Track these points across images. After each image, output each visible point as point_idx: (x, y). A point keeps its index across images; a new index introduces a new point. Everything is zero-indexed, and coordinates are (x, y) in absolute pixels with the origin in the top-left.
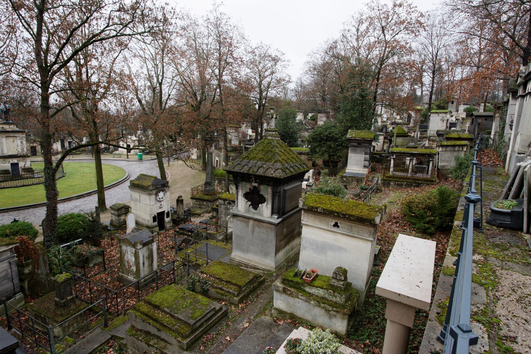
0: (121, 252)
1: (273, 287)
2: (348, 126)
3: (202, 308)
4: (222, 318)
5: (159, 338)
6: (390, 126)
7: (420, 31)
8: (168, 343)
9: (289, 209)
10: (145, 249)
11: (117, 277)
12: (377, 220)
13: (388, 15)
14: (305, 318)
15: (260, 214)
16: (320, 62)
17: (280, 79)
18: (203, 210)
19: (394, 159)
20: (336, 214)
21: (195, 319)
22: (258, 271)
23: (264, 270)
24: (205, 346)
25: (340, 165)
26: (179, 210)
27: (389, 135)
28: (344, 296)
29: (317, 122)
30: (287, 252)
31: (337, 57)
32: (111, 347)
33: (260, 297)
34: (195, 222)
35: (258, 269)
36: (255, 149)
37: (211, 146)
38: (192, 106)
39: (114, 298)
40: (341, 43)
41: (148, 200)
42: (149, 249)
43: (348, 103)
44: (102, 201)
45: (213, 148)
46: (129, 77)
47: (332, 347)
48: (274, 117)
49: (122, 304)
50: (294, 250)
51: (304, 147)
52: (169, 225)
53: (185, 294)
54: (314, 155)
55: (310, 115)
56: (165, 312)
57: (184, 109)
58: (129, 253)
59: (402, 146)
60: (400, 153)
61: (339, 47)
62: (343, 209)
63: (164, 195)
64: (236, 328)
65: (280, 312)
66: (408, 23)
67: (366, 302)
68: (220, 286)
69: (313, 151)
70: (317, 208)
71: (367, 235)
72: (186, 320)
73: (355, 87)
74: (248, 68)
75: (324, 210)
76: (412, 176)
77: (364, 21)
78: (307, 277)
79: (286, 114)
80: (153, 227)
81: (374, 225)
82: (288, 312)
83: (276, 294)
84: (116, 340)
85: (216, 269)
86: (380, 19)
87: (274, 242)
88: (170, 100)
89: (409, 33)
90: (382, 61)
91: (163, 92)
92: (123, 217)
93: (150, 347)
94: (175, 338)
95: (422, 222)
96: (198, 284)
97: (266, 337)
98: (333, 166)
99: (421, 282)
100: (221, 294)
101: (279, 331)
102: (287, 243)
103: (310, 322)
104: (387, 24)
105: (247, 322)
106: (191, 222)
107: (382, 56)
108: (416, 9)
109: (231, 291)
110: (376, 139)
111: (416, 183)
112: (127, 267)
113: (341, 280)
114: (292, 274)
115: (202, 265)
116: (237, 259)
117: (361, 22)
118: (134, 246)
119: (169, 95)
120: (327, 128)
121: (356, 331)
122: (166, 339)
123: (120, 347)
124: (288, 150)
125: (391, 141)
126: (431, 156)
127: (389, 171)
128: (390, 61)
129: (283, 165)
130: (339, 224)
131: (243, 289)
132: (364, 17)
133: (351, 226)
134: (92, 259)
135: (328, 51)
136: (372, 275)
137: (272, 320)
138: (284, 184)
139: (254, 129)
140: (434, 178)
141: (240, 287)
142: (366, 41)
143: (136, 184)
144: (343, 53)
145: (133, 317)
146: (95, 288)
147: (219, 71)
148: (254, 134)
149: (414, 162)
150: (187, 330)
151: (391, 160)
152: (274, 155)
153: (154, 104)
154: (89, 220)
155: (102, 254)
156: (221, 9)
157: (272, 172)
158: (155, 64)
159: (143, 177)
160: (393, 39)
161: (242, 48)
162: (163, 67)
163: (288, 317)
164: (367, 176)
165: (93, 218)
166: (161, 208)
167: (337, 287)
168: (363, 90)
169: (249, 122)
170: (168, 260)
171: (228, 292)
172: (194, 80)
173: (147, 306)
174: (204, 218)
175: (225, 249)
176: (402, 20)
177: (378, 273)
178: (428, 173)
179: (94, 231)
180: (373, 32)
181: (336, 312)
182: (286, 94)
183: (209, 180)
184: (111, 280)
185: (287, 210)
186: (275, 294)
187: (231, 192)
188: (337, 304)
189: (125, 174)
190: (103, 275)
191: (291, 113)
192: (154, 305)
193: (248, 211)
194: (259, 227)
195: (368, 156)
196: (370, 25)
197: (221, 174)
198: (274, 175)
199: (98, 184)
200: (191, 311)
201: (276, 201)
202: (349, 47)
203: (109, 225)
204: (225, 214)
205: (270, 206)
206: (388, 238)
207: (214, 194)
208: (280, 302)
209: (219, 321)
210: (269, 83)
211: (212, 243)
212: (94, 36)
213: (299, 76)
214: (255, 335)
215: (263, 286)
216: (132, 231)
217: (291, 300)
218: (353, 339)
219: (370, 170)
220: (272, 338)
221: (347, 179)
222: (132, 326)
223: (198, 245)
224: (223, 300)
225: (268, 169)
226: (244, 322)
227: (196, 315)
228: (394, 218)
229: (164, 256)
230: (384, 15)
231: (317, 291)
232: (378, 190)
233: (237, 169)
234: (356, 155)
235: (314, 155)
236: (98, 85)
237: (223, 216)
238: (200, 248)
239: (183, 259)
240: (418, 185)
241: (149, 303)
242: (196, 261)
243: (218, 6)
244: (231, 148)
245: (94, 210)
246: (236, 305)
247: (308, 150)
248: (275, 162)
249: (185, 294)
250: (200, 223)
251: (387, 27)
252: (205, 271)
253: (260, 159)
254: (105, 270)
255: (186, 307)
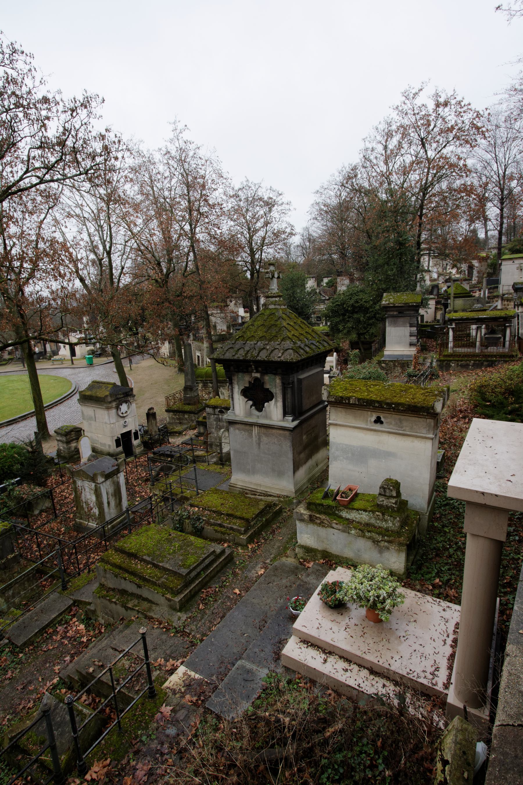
0: (76, 489)
1: (295, 516)
3: (196, 553)
6: (442, 285)
7: (479, 140)
8: (154, 603)
10: (108, 482)
11: (74, 525)
12: (438, 407)
13: (428, 121)
14: (345, 556)
15: (267, 417)
16: (334, 202)
17: (279, 231)
18: (185, 426)
19: (453, 328)
20: (377, 405)
21: (188, 568)
22: (271, 498)
23: (279, 496)
24: (206, 604)
25: (374, 346)
26: (151, 428)
27: (443, 298)
28: (398, 519)
29: (336, 288)
30: (310, 469)
31: (359, 190)
32: (74, 616)
33: (276, 533)
34: (174, 443)
35: (271, 496)
38: (157, 281)
39: (72, 554)
40: (363, 170)
41: (107, 417)
42: (114, 483)
44: (42, 425)
46: (64, 246)
47: (387, 587)
49: (84, 562)
50: (320, 467)
51: (321, 326)
52: (140, 450)
53: (170, 535)
54: (336, 335)
55: (326, 280)
56: (145, 561)
57: (146, 285)
58: (87, 490)
59: (464, 310)
60: (462, 319)
61: (359, 176)
62: (387, 396)
63: (129, 408)
64: (246, 577)
65: (308, 550)
66: (459, 129)
67: (431, 528)
68: (219, 522)
69: (334, 330)
70: (349, 398)
71: (424, 431)
72: (175, 569)
73: (388, 231)
74: (232, 220)
75: (359, 400)
76: (482, 352)
77: (394, 134)
78: (342, 497)
80: (118, 454)
81: (434, 415)
82: (320, 548)
83: (299, 525)
84: (80, 606)
85: (211, 499)
86: (416, 128)
87: (290, 456)
88: (124, 274)
89: (461, 145)
90: (424, 189)
91: (114, 265)
92: (73, 445)
94: (163, 596)
95: (503, 411)
96: (187, 521)
97: (291, 586)
98: (365, 349)
99: (514, 475)
101: (308, 575)
102: (309, 457)
104: (429, 133)
105: (261, 568)
106: (169, 443)
107: (424, 182)
108: (469, 107)
109: (235, 527)
110: (423, 304)
111: (488, 361)
112: (86, 510)
114: (320, 495)
117: (389, 135)
118: (93, 479)
119: (123, 268)
120: (351, 294)
121: (420, 568)
122: (150, 598)
123: (86, 614)
124: (299, 322)
125: (446, 306)
126: (508, 319)
127: (447, 347)
128: (437, 188)
129: (295, 343)
130: (382, 419)
131: (252, 523)
132: (394, 127)
133: (400, 420)
134: (37, 504)
135: (345, 182)
136: (436, 491)
137: (297, 562)
139: (247, 307)
140: (513, 351)
141: (247, 520)
142: (399, 162)
143: (88, 396)
144: (366, 185)
145: (102, 572)
146: (45, 542)
148: (248, 315)
149: (483, 331)
151: (448, 333)
152: (280, 330)
153: (103, 283)
154: (28, 451)
155: (50, 495)
156: (186, 136)
157: (280, 355)
158: (98, 226)
159: (95, 385)
160: (438, 156)
161: (220, 190)
162: (110, 228)
163: (319, 556)
164: (416, 357)
165: (32, 447)
166: (125, 426)
167: (387, 507)
168: (400, 235)
169: (239, 298)
171: (232, 529)
172: (155, 244)
173: (118, 555)
174: (187, 437)
175: (220, 473)
176: (450, 126)
177: (443, 487)
178: (504, 346)
179: (35, 466)
180: (410, 147)
181: (389, 542)
182: (288, 254)
183: (189, 384)
184: (65, 530)
186: (298, 524)
188: (388, 531)
189: (71, 386)
190: (54, 525)
191: (298, 279)
192: (129, 553)
193: (250, 415)
194: (267, 435)
195: (415, 328)
196: (403, 138)
198: (282, 358)
199: (35, 402)
200: (181, 558)
201: (289, 396)
202: (374, 174)
203: (55, 457)
204: (217, 427)
205: (280, 404)
206: (454, 439)
207: (199, 402)
208: (306, 536)
209: (222, 569)
210: (264, 239)
211: (201, 467)
212: (10, 188)
213: (305, 225)
215: (280, 518)
216: (89, 460)
217: (322, 532)
218: (416, 579)
219: (419, 348)
221: (387, 364)
222: (101, 584)
223: (183, 472)
224: (225, 541)
225: (272, 351)
226: (257, 568)
227: (189, 562)
228: (461, 411)
230: (422, 122)
231: (358, 516)
232: (433, 375)
233: (228, 356)
234: (398, 329)
236: (22, 258)
237: (213, 430)
239: (163, 492)
240: (491, 364)
241: (121, 551)
242: (182, 492)
243: (181, 132)
244: (217, 337)
245: (33, 437)
246: (244, 547)
247: (327, 329)
248: (282, 340)
249: (170, 535)
250: (182, 443)
251: (429, 139)
252: (196, 503)
253: (261, 338)
254: (56, 516)
255: (174, 552)
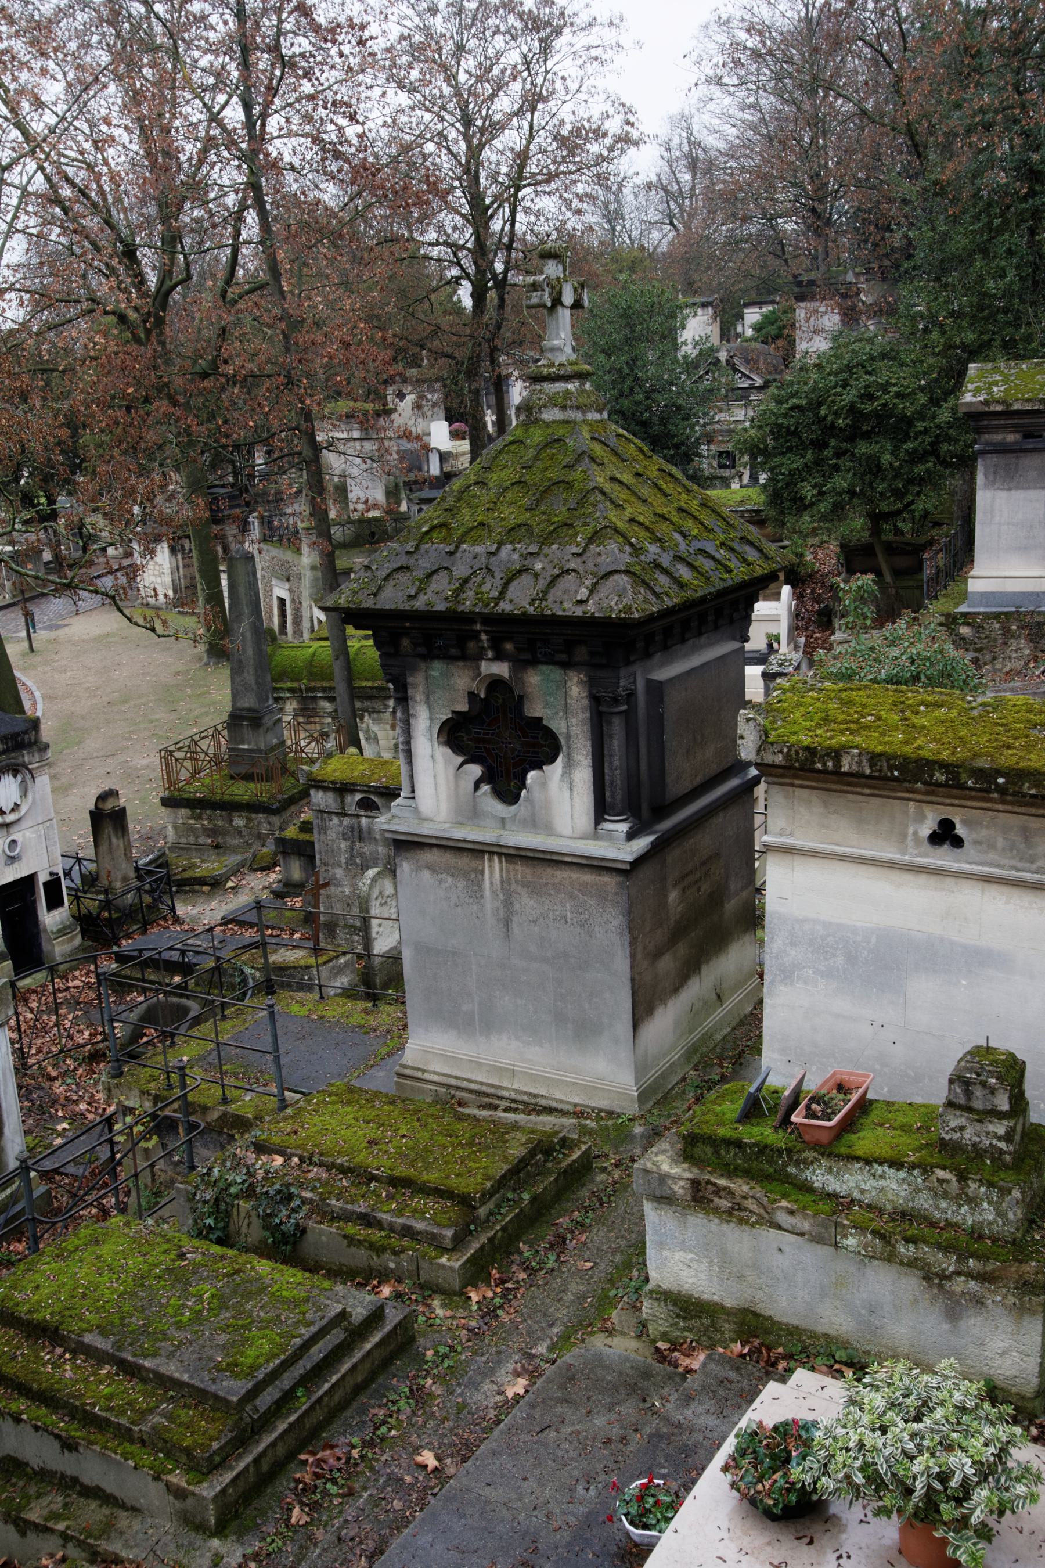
1: (638, 1183)
2: (964, 347)
3: (277, 1321)
4: (386, 1363)
5: (69, 1484)
8: (123, 1506)
9: (685, 785)
14: (822, 1327)
15: (535, 823)
17: (577, 131)
18: (235, 859)
20: (939, 777)
23: (580, 1113)
24: (315, 1506)
25: (932, 562)
28: (1016, 1194)
29: (792, 343)
30: (696, 1013)
33: (571, 1245)
34: (195, 920)
35: (550, 1110)
36: (481, 483)
37: (244, 527)
38: (122, 318)
43: (955, 220)
45: (256, 532)
47: (976, 1443)
48: (568, 298)
50: (729, 1004)
51: (735, 486)
52: (67, 948)
53: (182, 1256)
54: (790, 520)
55: (753, 316)
56: (88, 1351)
63: (24, 793)
64: (463, 1406)
68: (361, 1207)
70: (836, 754)
72: (202, 1381)
73: (988, 127)
74: (401, 86)
75: (874, 758)
78: (810, 1114)
79: (626, 315)
82: (729, 1303)
87: (622, 964)
93: (31, 1536)
94: (157, 1478)
96: (244, 1205)
98: (897, 573)
100: (372, 1246)
101: (688, 1399)
102: (691, 967)
103: (845, 1345)
105: (517, 1374)
106: (177, 920)
109: (420, 1226)
113: (995, 1114)
114: (731, 1108)
115: (259, 1118)
116: (437, 1068)
120: (849, 368)
122: (109, 1488)
124: (653, 473)
129: (637, 551)
130: (960, 830)
137: (649, 1352)
138: (648, 655)
141: (464, 1201)
147: (247, 107)
148: (465, 446)
150: (213, 1429)
152: (582, 502)
166: (12, 860)
167: (978, 1153)
169: (429, 382)
170: (74, 1118)
171: (407, 1232)
174: (243, 899)
175: (365, 1030)
181: (983, 1278)
182: (613, 216)
183: (248, 702)
185: (676, 787)
187: (369, 750)
188: (981, 1237)
191: (651, 310)
192: (29, 1323)
194: (535, 890)
197: (311, 663)
198: (591, 607)
200: (222, 1338)
201: (616, 744)
205: (583, 775)
207: (285, 770)
208: (679, 1256)
210: (522, 157)
211: (295, 1008)
213: (677, 104)
214: (567, 1430)
215: (584, 1193)
220: (657, 1435)
221: (979, 628)
223: (226, 1025)
224: (384, 1277)
225: (555, 578)
226: (502, 1375)
227: (251, 1353)
229: (55, 1102)
231: (869, 1184)
233: (392, 598)
234: (1019, 495)
235: (790, 520)
237: (339, 873)
238: (237, 1037)
239: (157, 1099)
242: (225, 1101)
244: (350, 531)
246: (456, 1296)
247: (756, 498)
248: (590, 541)
249: (182, 1256)
250: (225, 921)
252: (276, 1139)
253: (513, 533)
